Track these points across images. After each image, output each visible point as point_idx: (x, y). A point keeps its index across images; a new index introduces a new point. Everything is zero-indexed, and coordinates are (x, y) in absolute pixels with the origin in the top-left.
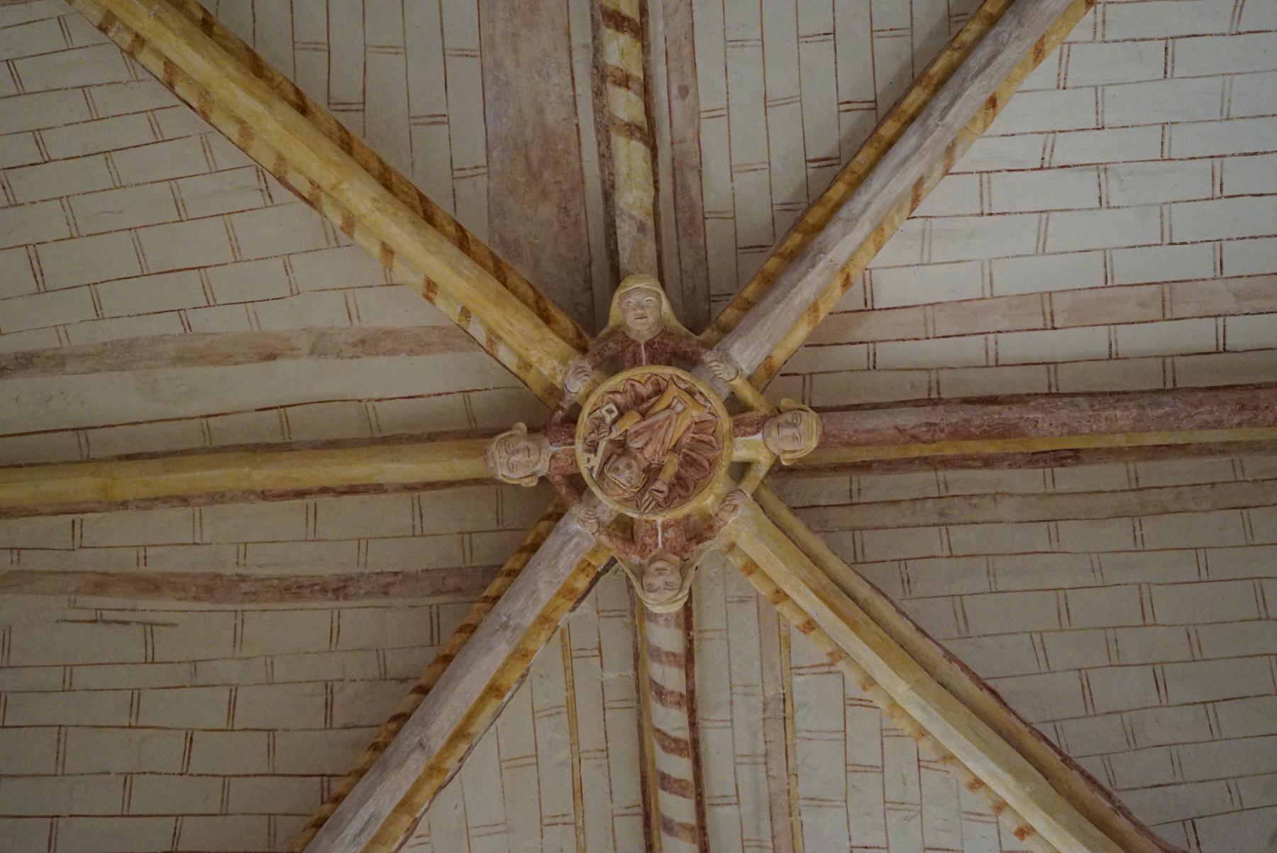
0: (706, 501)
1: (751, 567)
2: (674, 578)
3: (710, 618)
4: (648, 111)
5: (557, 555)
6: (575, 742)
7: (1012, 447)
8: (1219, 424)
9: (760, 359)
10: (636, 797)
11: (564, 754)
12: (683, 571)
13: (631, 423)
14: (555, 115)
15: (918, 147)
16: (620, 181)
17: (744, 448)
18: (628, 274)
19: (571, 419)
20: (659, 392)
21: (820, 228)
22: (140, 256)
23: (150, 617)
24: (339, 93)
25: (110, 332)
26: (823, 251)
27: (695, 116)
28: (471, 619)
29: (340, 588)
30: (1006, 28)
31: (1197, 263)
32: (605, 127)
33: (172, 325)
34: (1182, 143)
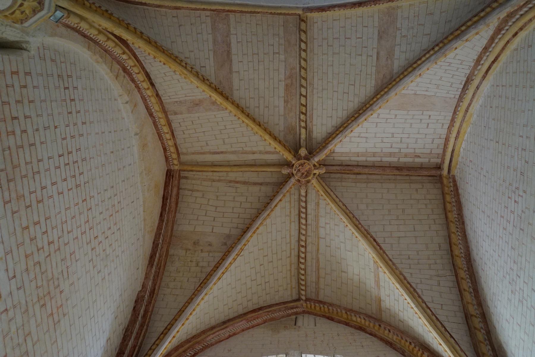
0: (310, 178)
1: (315, 187)
2: (305, 188)
3: (309, 191)
4: (306, 125)
5: (289, 184)
6: (290, 206)
7: (352, 172)
8: (379, 172)
9: (319, 159)
10: (298, 213)
11: (289, 207)
12: (306, 186)
13: (300, 167)
14: (293, 124)
15: (341, 136)
16: (301, 134)
17: (316, 172)
18: (302, 147)
19: (293, 165)
20: (305, 163)
21: (328, 144)
22: (237, 140)
23: (236, 186)
24: (265, 121)
25: (233, 149)
26: (328, 147)
27: (312, 125)
28: (278, 191)
29: (261, 184)
30: (354, 123)
31: (379, 150)
32: (300, 126)
33: (241, 149)
34: (378, 135)
